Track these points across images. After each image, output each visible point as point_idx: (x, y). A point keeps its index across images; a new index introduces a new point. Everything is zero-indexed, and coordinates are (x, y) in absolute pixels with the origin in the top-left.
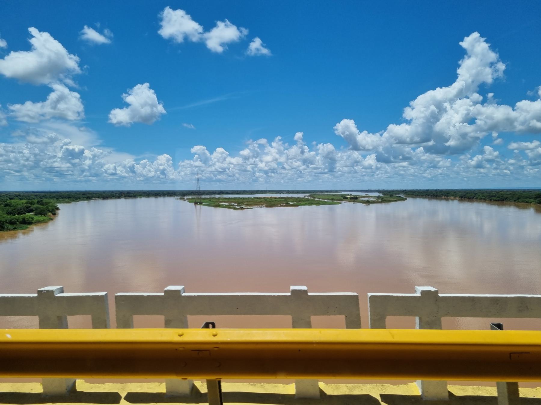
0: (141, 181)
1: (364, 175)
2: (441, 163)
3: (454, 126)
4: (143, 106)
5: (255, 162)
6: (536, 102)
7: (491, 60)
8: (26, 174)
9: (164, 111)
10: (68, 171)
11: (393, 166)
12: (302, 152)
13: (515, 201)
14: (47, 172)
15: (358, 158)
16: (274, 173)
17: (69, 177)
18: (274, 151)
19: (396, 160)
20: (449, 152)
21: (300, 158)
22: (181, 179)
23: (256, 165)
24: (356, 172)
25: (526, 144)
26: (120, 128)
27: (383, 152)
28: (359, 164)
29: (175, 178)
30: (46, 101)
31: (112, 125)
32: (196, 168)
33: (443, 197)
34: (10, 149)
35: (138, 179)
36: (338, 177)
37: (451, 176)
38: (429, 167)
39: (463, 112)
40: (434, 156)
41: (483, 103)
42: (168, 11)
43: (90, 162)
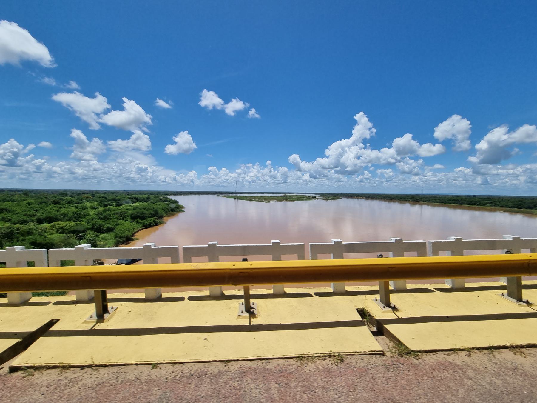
2: (342, 179)
3: (350, 160)
4: (185, 143)
6: (391, 149)
7: (369, 127)
8: (114, 180)
9: (196, 147)
10: (138, 179)
12: (271, 172)
13: (399, 200)
14: (126, 179)
15: (300, 175)
16: (254, 182)
17: (139, 183)
19: (320, 177)
20: (347, 173)
21: (269, 174)
22: (202, 185)
23: (244, 178)
24: (298, 183)
27: (313, 173)
28: (300, 179)
29: (199, 184)
30: (129, 139)
31: (166, 154)
33: (356, 197)
35: (178, 184)
36: (288, 186)
37: (347, 186)
38: (336, 181)
39: (355, 152)
40: (340, 175)
42: (205, 92)
43: (151, 174)
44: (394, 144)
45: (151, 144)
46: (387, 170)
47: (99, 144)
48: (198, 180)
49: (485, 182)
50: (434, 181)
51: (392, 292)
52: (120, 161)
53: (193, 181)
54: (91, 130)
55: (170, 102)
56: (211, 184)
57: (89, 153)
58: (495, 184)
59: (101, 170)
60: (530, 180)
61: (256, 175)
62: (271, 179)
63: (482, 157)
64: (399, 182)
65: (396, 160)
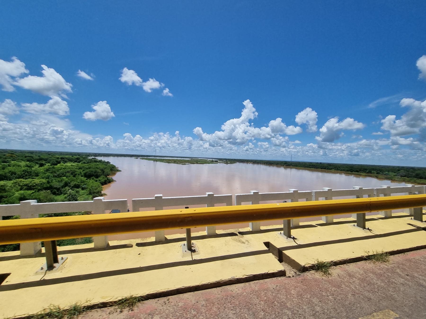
0: (96, 148)
1: (203, 151)
2: (234, 148)
3: (240, 134)
4: (103, 112)
5: (156, 142)
7: (253, 111)
8: (25, 141)
9: (114, 116)
11: (215, 148)
12: (179, 140)
13: (276, 164)
15: (202, 144)
16: (164, 148)
17: (53, 144)
19: (217, 146)
23: (156, 144)
24: (200, 150)
25: (264, 143)
26: (89, 122)
27: (212, 142)
31: (85, 119)
32: (126, 144)
34: (18, 127)
35: (94, 147)
40: (232, 145)
41: (250, 126)
44: (270, 125)
46: (265, 142)
47: (12, 106)
48: (114, 144)
49: (325, 154)
50: (295, 152)
53: (109, 144)
55: (92, 74)
56: (126, 148)
58: (330, 156)
59: (12, 130)
60: (350, 153)
61: (166, 142)
62: (179, 146)
63: (323, 137)
65: (271, 136)
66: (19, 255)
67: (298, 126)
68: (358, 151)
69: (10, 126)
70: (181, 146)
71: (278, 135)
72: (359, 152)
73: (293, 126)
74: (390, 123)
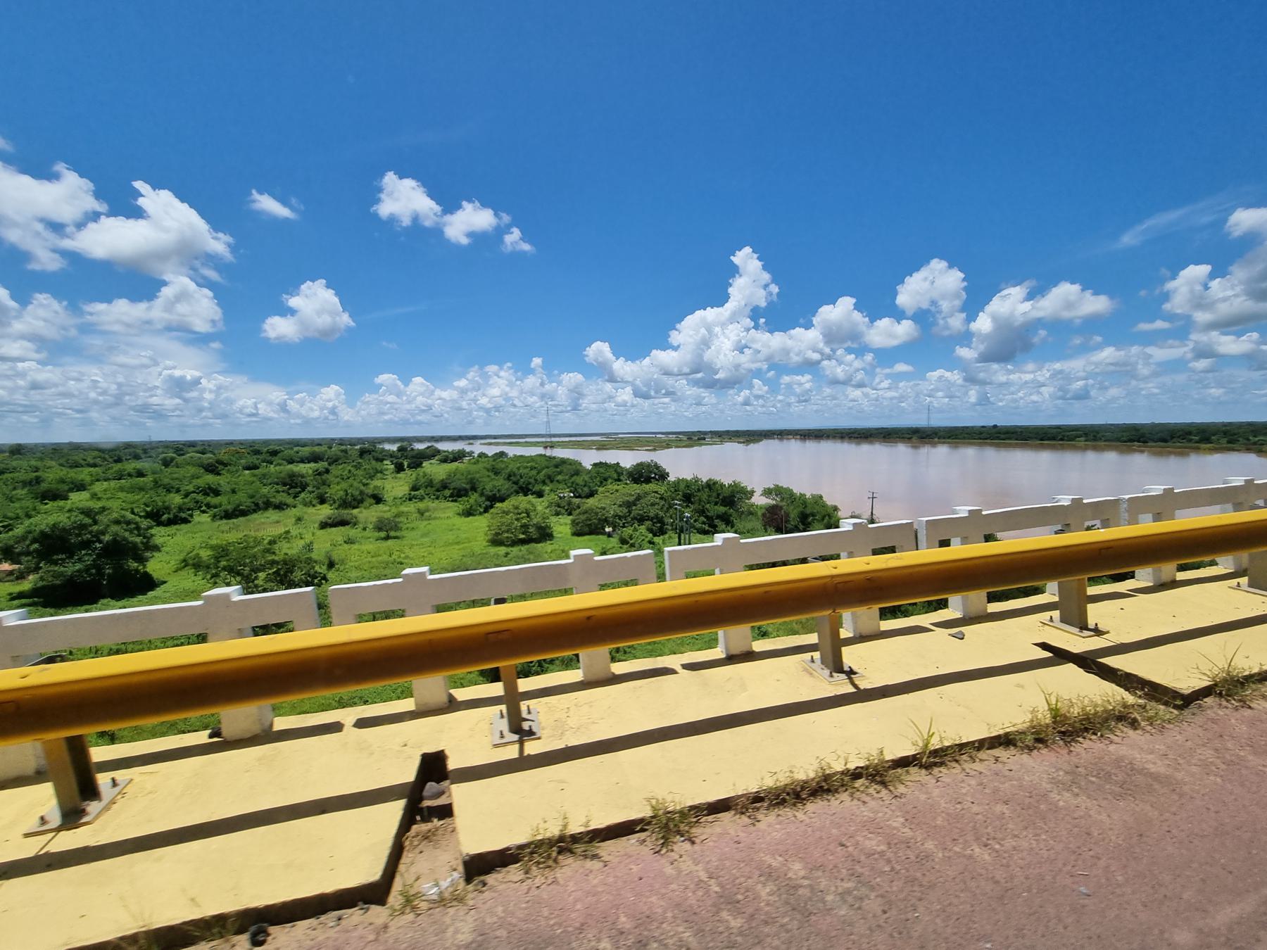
1: (615, 415)
2: (706, 399)
3: (725, 355)
4: (319, 313)
7: (764, 282)
8: (94, 415)
9: (353, 324)
12: (542, 384)
13: (884, 437)
16: (499, 411)
18: (502, 382)
19: (658, 395)
23: (475, 400)
24: (606, 410)
25: (799, 378)
26: (283, 348)
27: (641, 385)
29: (352, 419)
34: (75, 374)
35: (292, 421)
37: (715, 415)
39: (734, 338)
40: (701, 390)
41: (756, 327)
42: (390, 178)
44: (815, 320)
45: (223, 313)
46: (803, 376)
47: (56, 312)
48: (349, 410)
49: (984, 400)
50: (891, 399)
51: (849, 642)
52: (122, 359)
53: (336, 410)
54: (33, 272)
55: (293, 201)
56: (386, 417)
57: (23, 337)
58: (1000, 404)
59: (56, 385)
60: (1060, 393)
61: (506, 394)
62: (543, 403)
63: (982, 347)
64: (824, 402)
65: (822, 354)
66: (582, 682)
67: (907, 319)
68: (1086, 385)
69: (46, 374)
70: (550, 403)
71: (839, 352)
72: (1089, 388)
73: (892, 319)
74: (1192, 291)
